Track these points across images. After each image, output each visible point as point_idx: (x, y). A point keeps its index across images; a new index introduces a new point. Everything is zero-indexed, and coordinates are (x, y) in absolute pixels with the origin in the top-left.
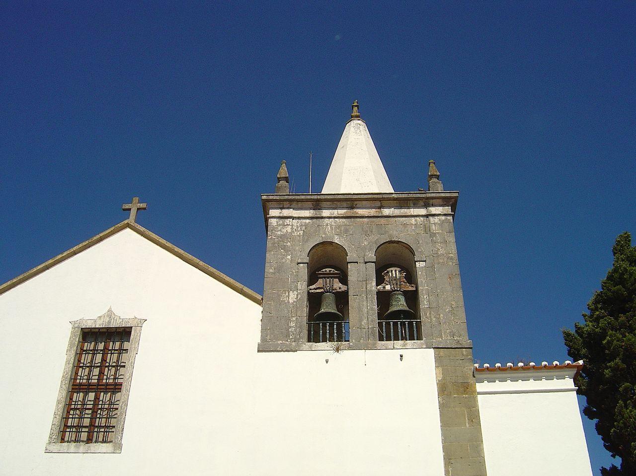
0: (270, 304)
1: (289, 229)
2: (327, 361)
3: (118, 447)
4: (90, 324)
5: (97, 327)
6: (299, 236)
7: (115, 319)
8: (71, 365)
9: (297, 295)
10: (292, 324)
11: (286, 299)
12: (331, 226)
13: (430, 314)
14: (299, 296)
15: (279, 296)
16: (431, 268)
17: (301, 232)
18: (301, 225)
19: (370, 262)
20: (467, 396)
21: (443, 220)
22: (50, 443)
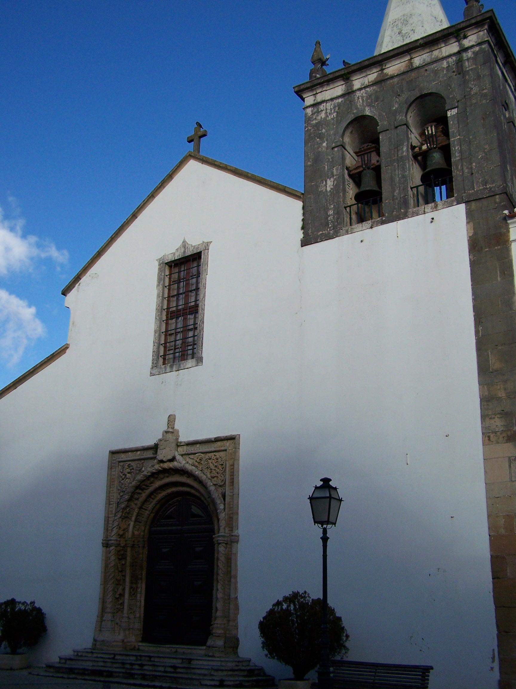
0: (310, 198)
1: (323, 115)
2: (362, 241)
3: (200, 360)
4: (171, 258)
5: (176, 259)
6: (333, 119)
7: (189, 247)
8: (161, 298)
9: (334, 181)
10: (331, 212)
11: (323, 189)
12: (362, 97)
13: (462, 166)
14: (335, 182)
15: (317, 187)
16: (462, 116)
17: (335, 114)
18: (335, 107)
19: (400, 126)
20: (499, 247)
21: (478, 52)
22: (152, 368)
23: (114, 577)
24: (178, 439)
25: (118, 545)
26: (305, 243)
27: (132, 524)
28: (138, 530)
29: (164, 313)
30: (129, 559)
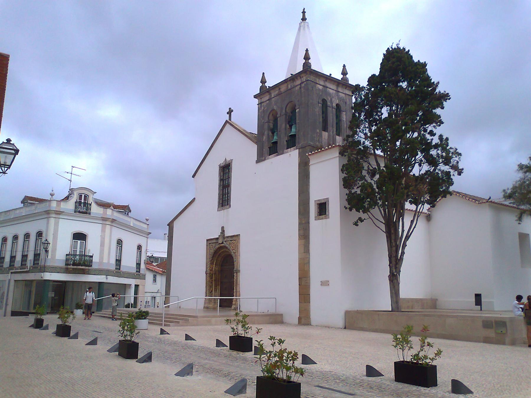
3: (230, 206)
23: (209, 285)
24: (224, 235)
25: (210, 273)
26: (258, 162)
27: (214, 266)
28: (217, 268)
29: (221, 187)
30: (214, 278)
